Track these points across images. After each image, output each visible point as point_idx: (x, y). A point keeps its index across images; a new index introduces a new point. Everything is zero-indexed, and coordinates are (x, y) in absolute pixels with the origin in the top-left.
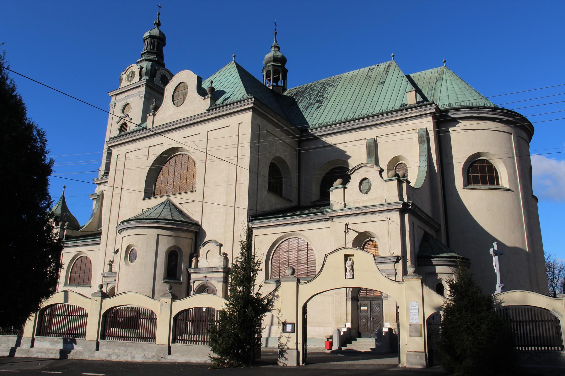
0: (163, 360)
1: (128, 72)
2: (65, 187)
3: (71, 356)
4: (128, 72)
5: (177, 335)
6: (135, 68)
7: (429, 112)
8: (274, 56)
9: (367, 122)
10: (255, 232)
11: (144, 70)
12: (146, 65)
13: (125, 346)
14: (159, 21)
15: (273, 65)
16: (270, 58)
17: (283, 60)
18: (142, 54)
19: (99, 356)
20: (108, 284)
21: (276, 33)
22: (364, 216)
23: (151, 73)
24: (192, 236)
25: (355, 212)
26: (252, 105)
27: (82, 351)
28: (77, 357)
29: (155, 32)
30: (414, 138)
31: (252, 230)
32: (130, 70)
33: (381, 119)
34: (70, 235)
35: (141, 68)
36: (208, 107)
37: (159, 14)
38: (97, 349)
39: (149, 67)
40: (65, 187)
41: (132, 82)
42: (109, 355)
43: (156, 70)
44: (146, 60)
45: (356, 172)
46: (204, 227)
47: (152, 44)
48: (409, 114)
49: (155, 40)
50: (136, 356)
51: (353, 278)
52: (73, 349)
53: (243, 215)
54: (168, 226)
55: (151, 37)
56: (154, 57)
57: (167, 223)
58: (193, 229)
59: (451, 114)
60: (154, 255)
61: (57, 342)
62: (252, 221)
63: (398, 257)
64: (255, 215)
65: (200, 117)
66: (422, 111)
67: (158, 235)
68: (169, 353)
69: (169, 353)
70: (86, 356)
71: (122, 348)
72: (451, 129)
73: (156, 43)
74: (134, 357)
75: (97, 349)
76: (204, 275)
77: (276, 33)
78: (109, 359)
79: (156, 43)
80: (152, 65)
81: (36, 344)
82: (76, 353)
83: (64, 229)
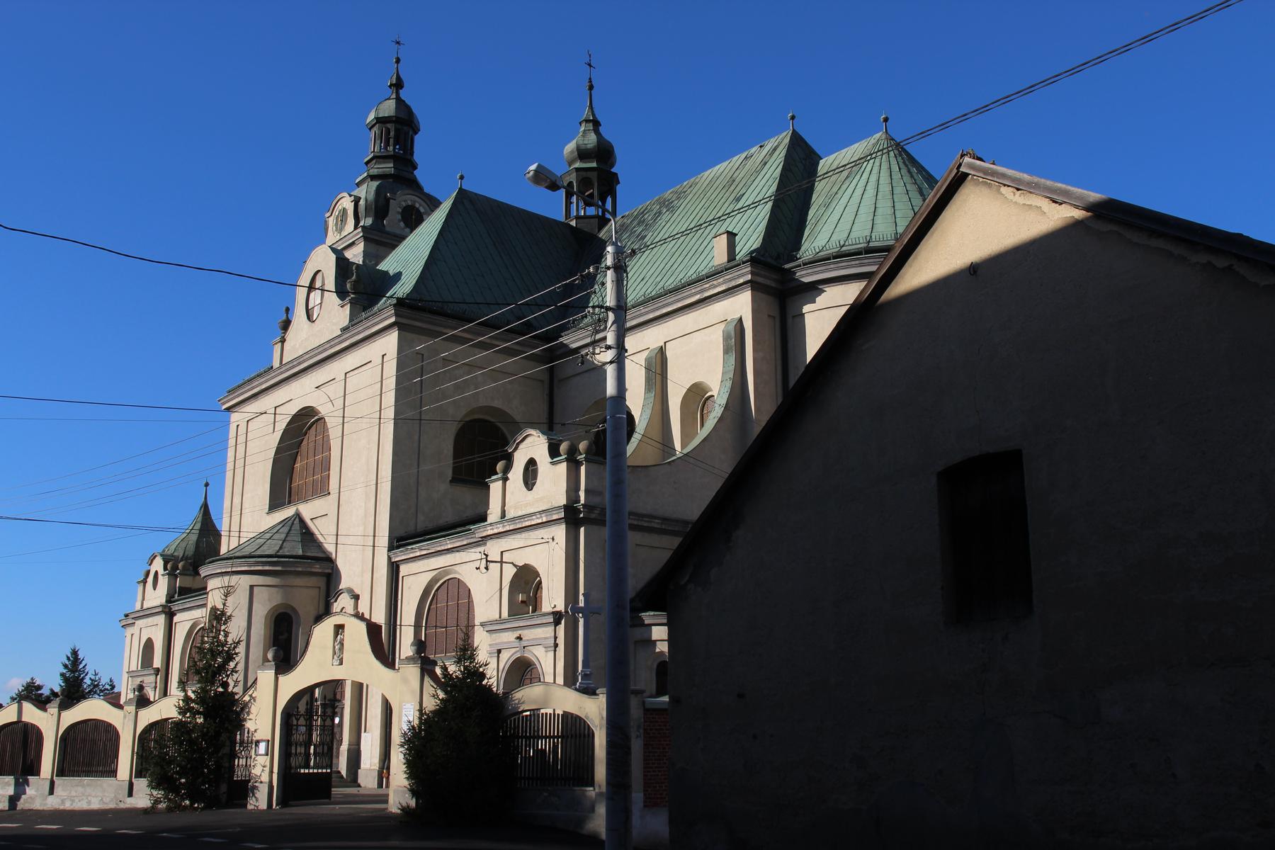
0: (122, 806)
1: (336, 213)
2: (207, 485)
3: (22, 805)
4: (336, 213)
5: (65, 767)
6: (347, 203)
7: (741, 281)
8: (578, 148)
9: (647, 313)
10: (403, 569)
11: (362, 202)
12: (366, 192)
13: (83, 786)
14: (399, 78)
15: (577, 170)
16: (572, 152)
17: (603, 153)
18: (367, 163)
19: (52, 803)
20: (499, 651)
21: (591, 88)
22: (524, 535)
23: (379, 208)
24: (321, 582)
25: (508, 528)
26: (393, 320)
27: (37, 796)
28: (27, 806)
29: (388, 108)
30: (715, 340)
31: (398, 567)
32: (339, 207)
33: (667, 305)
34: (188, 585)
35: (356, 201)
36: (346, 322)
37: (398, 61)
38: (51, 792)
39: (371, 196)
40: (207, 485)
41: (344, 234)
42: (63, 802)
43: (388, 200)
44: (373, 178)
45: (521, 446)
46: (340, 563)
47: (385, 138)
48: (709, 288)
49: (389, 126)
50: (93, 800)
51: (341, 663)
52: (25, 793)
53: (383, 540)
54: (267, 568)
55: (380, 121)
56: (388, 167)
57: (257, 563)
58: (317, 568)
59: (803, 276)
60: (245, 624)
61: (8, 784)
62: (398, 547)
63: (560, 612)
64: (398, 541)
65: (332, 347)
66: (730, 280)
67: (252, 587)
68: (130, 794)
69: (130, 794)
70: (37, 805)
71: (80, 789)
72: (806, 309)
73: (392, 134)
74: (89, 803)
75: (51, 792)
76: (517, 634)
77: (591, 88)
78: (62, 807)
79: (392, 134)
80: (378, 189)
81: (57, 790)
82: (26, 801)
83: (176, 577)
